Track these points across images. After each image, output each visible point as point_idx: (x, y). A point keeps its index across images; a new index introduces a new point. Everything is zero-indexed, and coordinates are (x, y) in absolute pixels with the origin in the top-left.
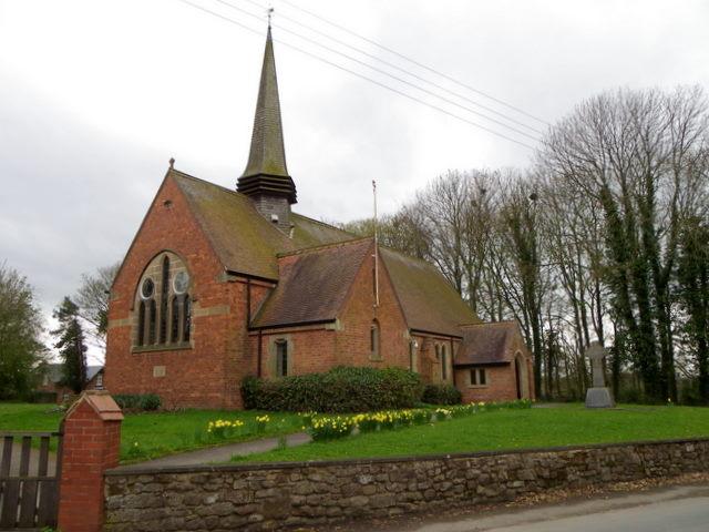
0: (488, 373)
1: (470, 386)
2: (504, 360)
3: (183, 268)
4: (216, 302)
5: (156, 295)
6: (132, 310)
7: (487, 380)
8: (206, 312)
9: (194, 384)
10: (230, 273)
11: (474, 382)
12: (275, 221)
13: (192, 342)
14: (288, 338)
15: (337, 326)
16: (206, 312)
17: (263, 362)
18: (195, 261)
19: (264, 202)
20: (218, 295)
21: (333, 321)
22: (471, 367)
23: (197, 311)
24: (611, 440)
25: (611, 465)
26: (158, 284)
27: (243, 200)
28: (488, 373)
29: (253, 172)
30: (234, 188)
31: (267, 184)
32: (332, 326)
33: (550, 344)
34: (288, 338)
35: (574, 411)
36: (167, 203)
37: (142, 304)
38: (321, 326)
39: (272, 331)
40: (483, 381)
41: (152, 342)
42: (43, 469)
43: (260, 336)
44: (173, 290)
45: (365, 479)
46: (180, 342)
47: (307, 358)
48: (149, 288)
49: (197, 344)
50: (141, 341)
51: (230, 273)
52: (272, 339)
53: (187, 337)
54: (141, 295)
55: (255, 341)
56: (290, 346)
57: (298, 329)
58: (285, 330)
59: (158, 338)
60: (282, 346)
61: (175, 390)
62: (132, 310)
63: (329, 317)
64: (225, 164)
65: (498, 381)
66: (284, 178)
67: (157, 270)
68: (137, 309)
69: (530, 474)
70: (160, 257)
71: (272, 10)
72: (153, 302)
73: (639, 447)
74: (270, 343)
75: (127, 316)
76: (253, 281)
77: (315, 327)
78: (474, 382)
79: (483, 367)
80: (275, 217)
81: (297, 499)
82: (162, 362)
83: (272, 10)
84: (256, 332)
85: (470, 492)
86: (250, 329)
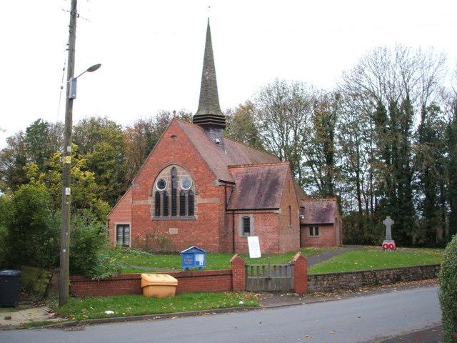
0: (320, 229)
1: (309, 236)
2: (330, 222)
4: (212, 196)
5: (168, 188)
6: (151, 196)
7: (320, 233)
9: (198, 238)
10: (220, 181)
11: (311, 234)
12: (218, 143)
13: (196, 216)
14: (251, 216)
18: (195, 172)
19: (212, 131)
20: (213, 193)
21: (278, 209)
22: (311, 226)
23: (198, 200)
24: (319, 273)
25: (413, 274)
26: (168, 183)
28: (320, 229)
29: (203, 113)
32: (277, 211)
34: (251, 216)
35: (372, 251)
37: (158, 194)
38: (272, 211)
40: (317, 233)
41: (174, 213)
43: (233, 214)
44: (180, 187)
45: (354, 278)
46: (314, 236)
48: (162, 184)
50: (157, 213)
52: (241, 216)
53: (191, 212)
54: (156, 188)
55: (230, 216)
56: (252, 220)
57: (257, 212)
58: (249, 212)
59: (178, 210)
60: (247, 221)
62: (151, 196)
63: (276, 207)
65: (324, 234)
67: (168, 174)
68: (154, 195)
69: (391, 276)
70: (170, 167)
72: (165, 192)
73: (422, 268)
75: (147, 199)
78: (311, 234)
79: (317, 226)
80: (218, 140)
81: (341, 283)
82: (175, 226)
84: (231, 212)
86: (226, 210)
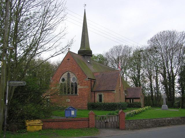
3: (74, 76)
4: (85, 85)
8: (82, 87)
10: (89, 78)
12: (89, 63)
13: (78, 94)
14: (102, 94)
15: (115, 92)
16: (82, 87)
17: (95, 99)
18: (78, 75)
21: (114, 91)
23: (79, 87)
25: (177, 121)
27: (80, 57)
30: (77, 53)
31: (85, 52)
33: (12, 52)
34: (102, 94)
35: (158, 110)
36: (68, 59)
39: (97, 92)
42: (115, 121)
43: (95, 93)
47: (107, 99)
48: (63, 80)
49: (79, 95)
51: (89, 78)
52: (98, 94)
53: (76, 92)
56: (103, 96)
60: (100, 96)
61: (73, 105)
64: (76, 49)
66: (90, 51)
70: (67, 73)
71: (85, 5)
74: (97, 95)
76: (92, 80)
77: (110, 92)
83: (85, 5)
85: (159, 125)
86: (91, 91)
